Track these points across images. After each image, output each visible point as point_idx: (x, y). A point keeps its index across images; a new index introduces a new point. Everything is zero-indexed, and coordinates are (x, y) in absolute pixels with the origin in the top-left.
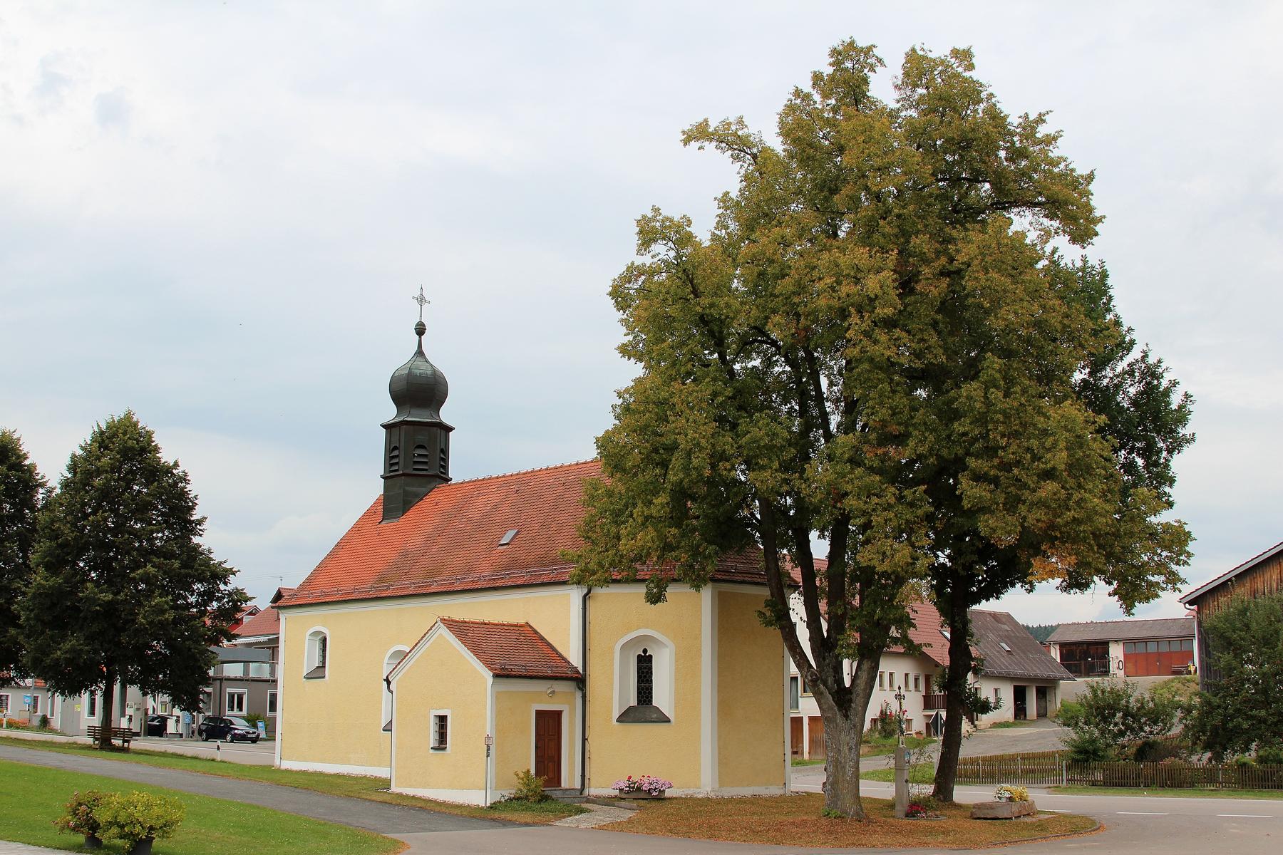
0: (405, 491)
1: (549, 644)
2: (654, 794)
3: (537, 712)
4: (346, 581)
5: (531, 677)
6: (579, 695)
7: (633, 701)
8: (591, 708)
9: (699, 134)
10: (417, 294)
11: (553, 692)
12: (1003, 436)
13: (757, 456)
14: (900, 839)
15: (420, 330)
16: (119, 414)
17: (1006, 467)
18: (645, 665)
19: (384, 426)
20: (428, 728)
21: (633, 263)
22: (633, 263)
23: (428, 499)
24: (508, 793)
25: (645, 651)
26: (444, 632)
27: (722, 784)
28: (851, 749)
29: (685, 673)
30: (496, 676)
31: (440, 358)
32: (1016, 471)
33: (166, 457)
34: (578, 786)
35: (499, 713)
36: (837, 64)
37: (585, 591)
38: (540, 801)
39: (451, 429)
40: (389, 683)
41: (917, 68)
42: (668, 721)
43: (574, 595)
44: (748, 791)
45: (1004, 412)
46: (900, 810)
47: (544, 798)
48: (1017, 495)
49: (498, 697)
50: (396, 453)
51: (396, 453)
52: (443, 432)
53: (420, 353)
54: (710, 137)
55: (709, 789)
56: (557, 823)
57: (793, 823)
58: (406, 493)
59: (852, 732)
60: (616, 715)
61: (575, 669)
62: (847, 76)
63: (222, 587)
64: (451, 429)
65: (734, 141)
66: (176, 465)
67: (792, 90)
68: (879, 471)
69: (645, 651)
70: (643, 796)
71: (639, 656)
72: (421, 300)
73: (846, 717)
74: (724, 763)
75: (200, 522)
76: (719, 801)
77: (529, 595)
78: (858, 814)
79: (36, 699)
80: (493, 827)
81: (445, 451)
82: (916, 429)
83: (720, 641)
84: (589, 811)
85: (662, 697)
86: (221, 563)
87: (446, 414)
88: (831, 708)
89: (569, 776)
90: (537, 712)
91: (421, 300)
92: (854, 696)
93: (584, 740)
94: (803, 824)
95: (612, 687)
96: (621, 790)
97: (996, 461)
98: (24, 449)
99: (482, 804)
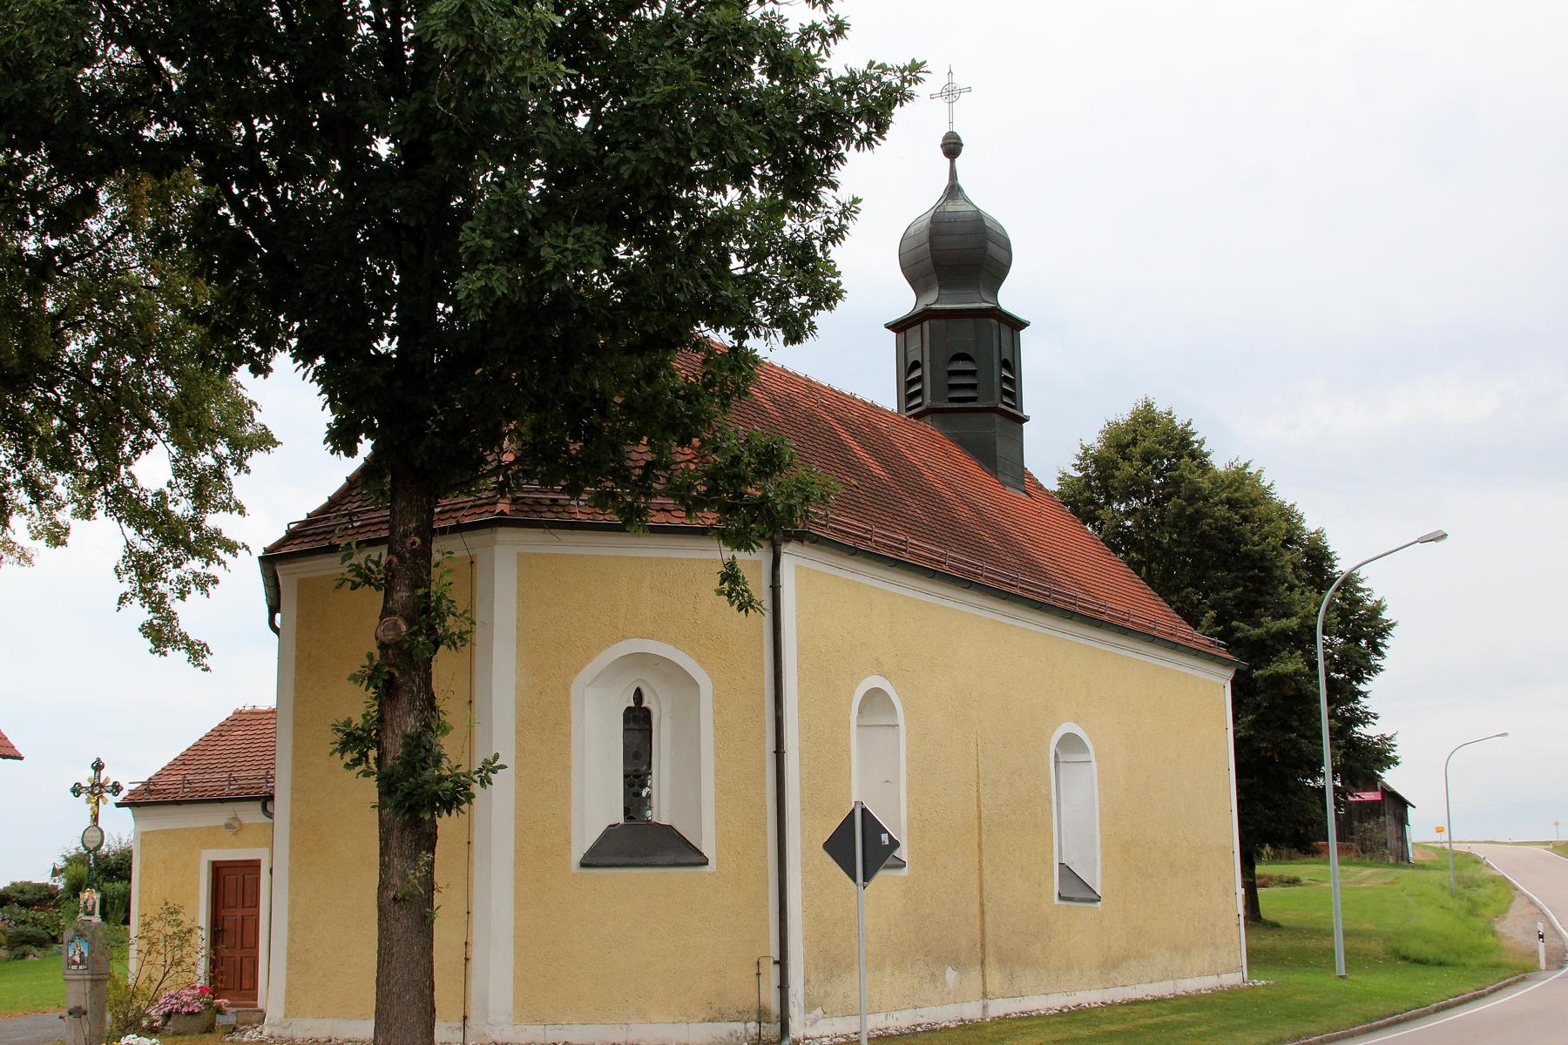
15: (952, 147)
16: (1122, 412)
19: (888, 326)
31: (988, 195)
39: (1022, 325)
51: (917, 373)
52: (1006, 333)
53: (953, 190)
60: (577, 854)
64: (1022, 325)
77: (987, 615)
81: (1011, 364)
87: (1009, 298)
90: (217, 869)
98: (1284, 494)
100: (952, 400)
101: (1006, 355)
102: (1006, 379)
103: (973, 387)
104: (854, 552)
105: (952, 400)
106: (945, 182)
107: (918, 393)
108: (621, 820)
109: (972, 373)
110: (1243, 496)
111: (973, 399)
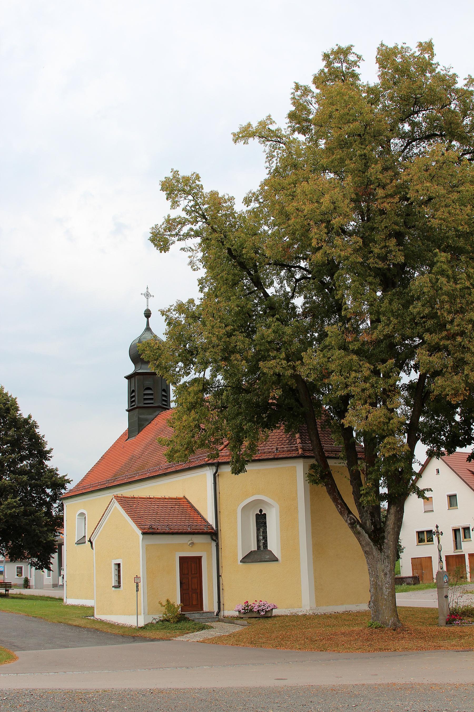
0: (138, 418)
1: (196, 510)
2: (262, 613)
3: (182, 559)
4: (107, 478)
5: (173, 533)
6: (214, 544)
7: (254, 547)
8: (223, 554)
9: (245, 134)
10: (144, 291)
11: (192, 543)
12: (449, 312)
13: (268, 351)
14: (422, 643)
17: (453, 337)
18: (261, 520)
19: (127, 377)
20: (111, 573)
21: (169, 216)
22: (169, 216)
23: (154, 422)
24: (158, 616)
25: (261, 511)
26: (117, 505)
27: (318, 603)
28: (386, 574)
29: (288, 525)
30: (144, 533)
32: (459, 339)
33: (24, 412)
34: (216, 610)
35: (148, 560)
36: (329, 64)
37: (215, 471)
38: (178, 622)
40: (91, 543)
41: (386, 57)
42: (277, 560)
43: (208, 473)
44: (340, 609)
45: (448, 294)
46: (442, 619)
47: (181, 619)
48: (463, 359)
49: (147, 549)
50: (133, 394)
51: (133, 394)
53: (148, 329)
54: (253, 135)
55: (308, 608)
56: (179, 638)
57: (343, 634)
58: (139, 419)
59: (386, 562)
60: (240, 557)
61: (209, 525)
62: (337, 71)
63: (63, 491)
65: (265, 133)
66: (30, 417)
67: (293, 86)
68: (357, 352)
69: (261, 511)
70: (255, 615)
71: (257, 514)
72: (148, 295)
73: (381, 550)
74: (319, 588)
75: (49, 452)
76: (315, 616)
77: (185, 477)
78: (395, 624)
79: (21, 568)
80: (123, 642)
82: (384, 315)
83: (312, 499)
84: (212, 627)
85: (273, 545)
86: (64, 476)
88: (368, 544)
89: (209, 602)
90: (182, 559)
91: (148, 295)
92: (386, 534)
93: (219, 576)
94: (350, 634)
95: (237, 537)
96: (239, 611)
97: (444, 333)
99: (134, 624)
100: (145, 404)
101: (164, 387)
102: (164, 396)
103: (152, 399)
104: (165, 475)
105: (145, 404)
106: (145, 326)
107: (134, 401)
108: (256, 549)
109: (152, 394)
110: (334, 502)
111: (152, 403)
